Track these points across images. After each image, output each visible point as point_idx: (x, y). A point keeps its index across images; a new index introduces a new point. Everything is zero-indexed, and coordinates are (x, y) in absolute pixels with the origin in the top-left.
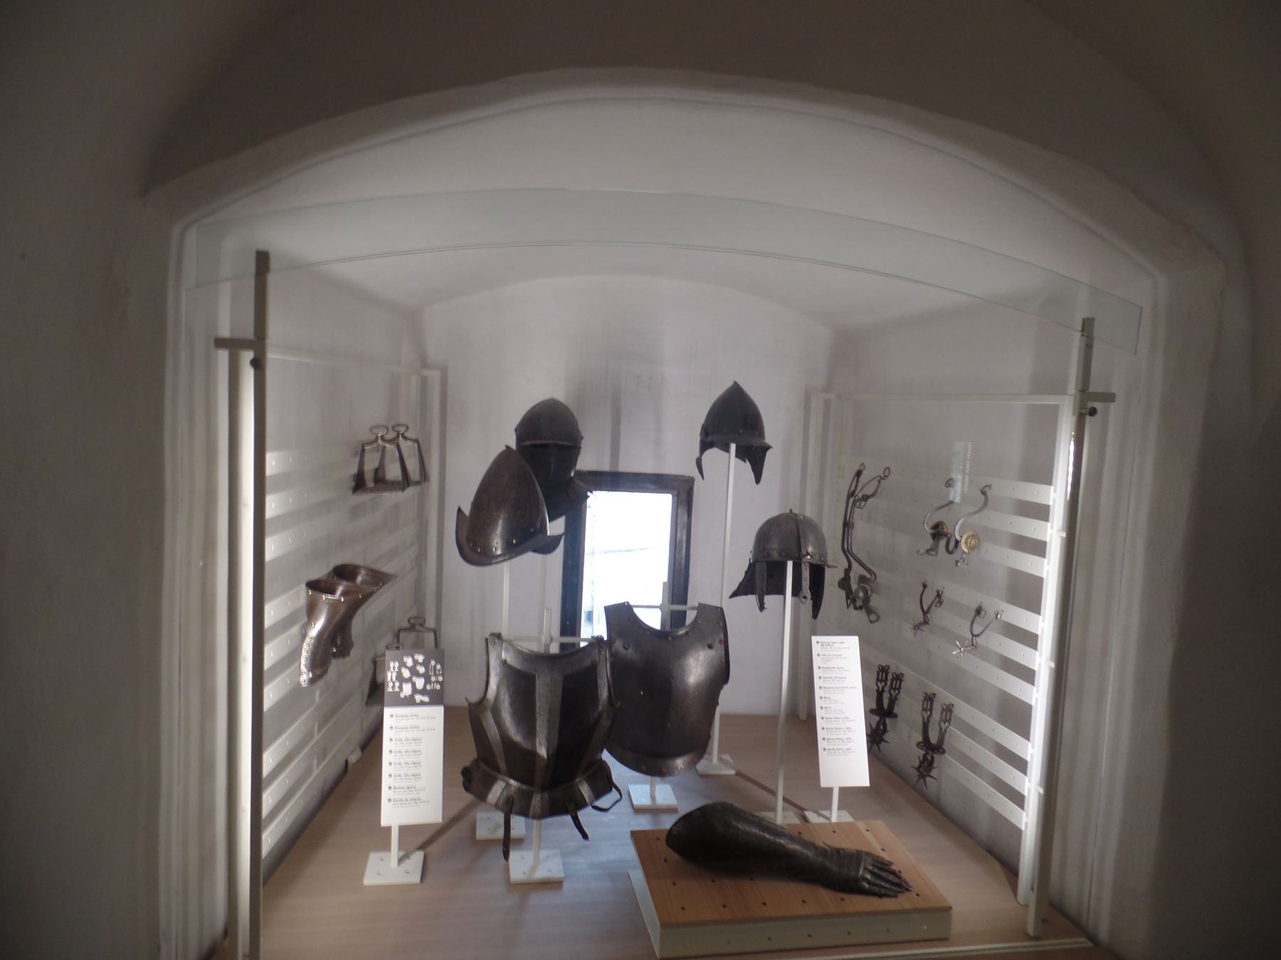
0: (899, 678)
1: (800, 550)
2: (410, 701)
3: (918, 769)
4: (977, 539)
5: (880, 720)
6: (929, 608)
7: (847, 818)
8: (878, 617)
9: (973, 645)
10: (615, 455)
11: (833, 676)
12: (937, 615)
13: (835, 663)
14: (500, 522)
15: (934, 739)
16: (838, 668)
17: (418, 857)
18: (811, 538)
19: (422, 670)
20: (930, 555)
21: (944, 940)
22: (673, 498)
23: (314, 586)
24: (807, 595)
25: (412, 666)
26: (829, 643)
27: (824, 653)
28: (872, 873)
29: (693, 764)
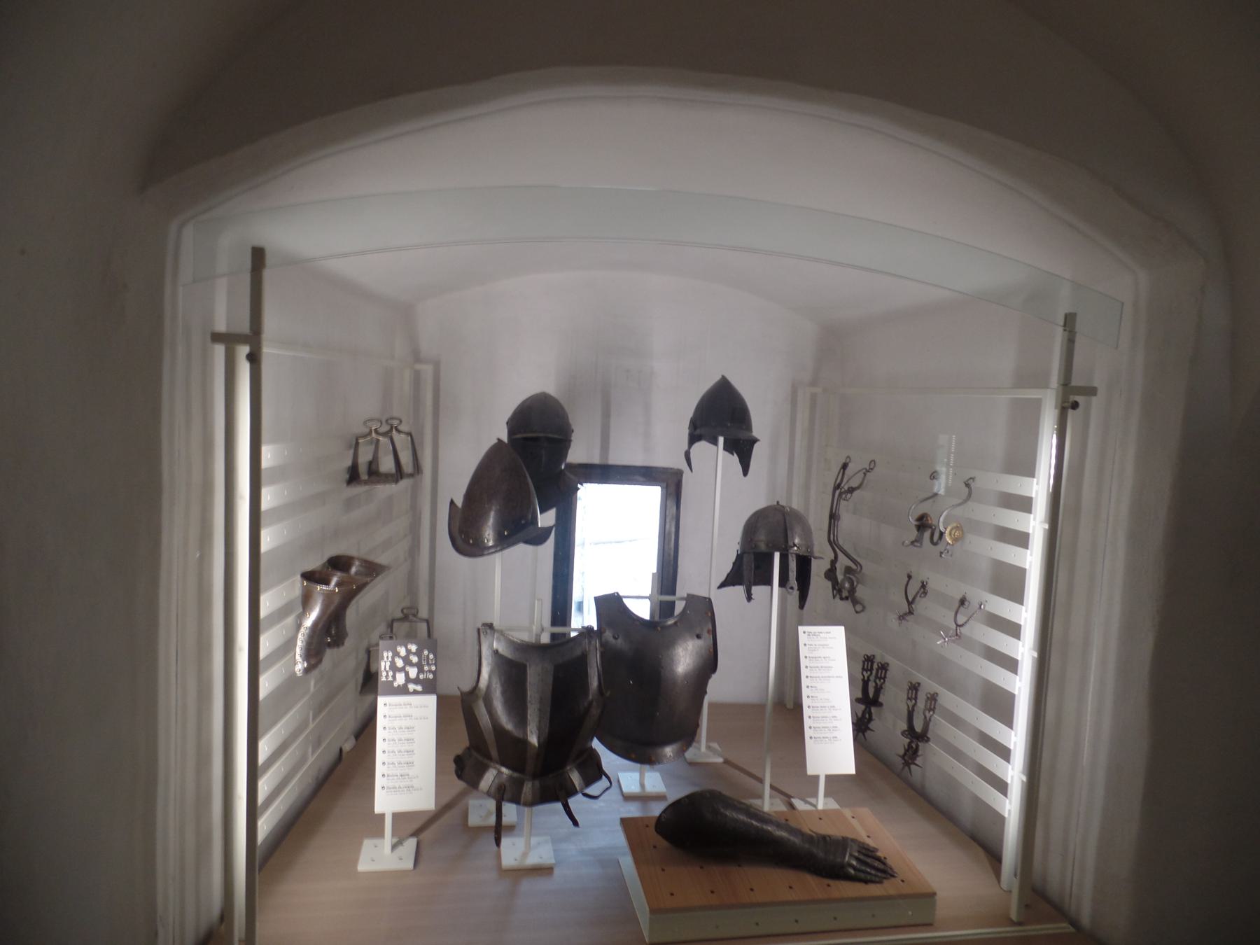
0: (884, 667)
1: (786, 541)
2: (403, 690)
3: (903, 757)
4: (961, 531)
5: (865, 709)
6: (914, 599)
7: (833, 805)
8: (864, 607)
9: (957, 635)
10: (605, 447)
11: (819, 665)
12: (922, 606)
13: (821, 652)
14: (492, 514)
15: (918, 727)
16: (824, 658)
17: (411, 843)
18: (798, 529)
19: (415, 659)
20: (915, 546)
21: (928, 925)
22: (662, 491)
23: (309, 576)
24: (794, 586)
25: (406, 656)
26: (815, 633)
27: (811, 643)
28: (857, 859)
29: (681, 752)
